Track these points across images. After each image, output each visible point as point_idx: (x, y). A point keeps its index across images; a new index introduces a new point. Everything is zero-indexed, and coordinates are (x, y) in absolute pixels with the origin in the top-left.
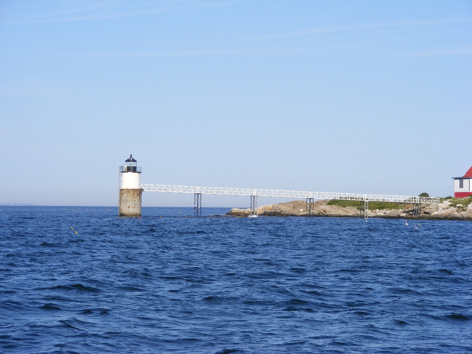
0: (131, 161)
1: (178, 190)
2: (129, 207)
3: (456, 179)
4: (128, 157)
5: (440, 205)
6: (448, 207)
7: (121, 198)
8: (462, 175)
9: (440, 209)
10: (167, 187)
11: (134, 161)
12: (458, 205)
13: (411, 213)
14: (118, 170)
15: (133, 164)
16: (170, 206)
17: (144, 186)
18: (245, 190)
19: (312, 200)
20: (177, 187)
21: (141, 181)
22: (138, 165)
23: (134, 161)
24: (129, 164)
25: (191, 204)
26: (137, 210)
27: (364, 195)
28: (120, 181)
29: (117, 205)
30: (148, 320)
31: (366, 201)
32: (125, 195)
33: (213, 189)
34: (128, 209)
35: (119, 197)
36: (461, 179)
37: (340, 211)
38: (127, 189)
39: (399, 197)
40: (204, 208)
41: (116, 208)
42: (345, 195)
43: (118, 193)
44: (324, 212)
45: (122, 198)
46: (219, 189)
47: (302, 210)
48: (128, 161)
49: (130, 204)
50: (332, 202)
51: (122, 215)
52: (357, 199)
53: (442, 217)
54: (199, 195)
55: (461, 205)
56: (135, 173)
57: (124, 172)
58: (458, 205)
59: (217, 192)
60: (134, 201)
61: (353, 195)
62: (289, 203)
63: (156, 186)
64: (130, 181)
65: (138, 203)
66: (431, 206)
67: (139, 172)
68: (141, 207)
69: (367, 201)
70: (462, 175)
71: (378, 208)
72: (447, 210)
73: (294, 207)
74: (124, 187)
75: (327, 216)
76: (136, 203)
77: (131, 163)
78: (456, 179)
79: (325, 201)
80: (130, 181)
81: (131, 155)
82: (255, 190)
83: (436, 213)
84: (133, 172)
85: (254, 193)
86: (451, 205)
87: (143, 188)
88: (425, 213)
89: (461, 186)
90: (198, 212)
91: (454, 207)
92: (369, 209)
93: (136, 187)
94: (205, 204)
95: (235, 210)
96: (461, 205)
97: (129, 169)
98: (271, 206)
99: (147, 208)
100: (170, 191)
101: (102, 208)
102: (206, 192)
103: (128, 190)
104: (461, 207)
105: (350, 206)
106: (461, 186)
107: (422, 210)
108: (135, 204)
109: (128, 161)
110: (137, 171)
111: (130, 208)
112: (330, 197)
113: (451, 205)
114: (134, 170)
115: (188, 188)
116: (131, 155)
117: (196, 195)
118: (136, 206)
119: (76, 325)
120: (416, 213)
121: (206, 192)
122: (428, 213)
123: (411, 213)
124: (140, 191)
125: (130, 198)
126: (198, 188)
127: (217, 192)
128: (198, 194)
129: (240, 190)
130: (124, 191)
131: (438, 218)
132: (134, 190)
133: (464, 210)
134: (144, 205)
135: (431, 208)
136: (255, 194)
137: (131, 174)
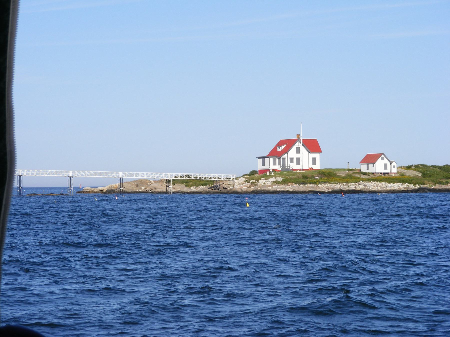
8: (265, 155)
9: (236, 185)
16: (28, 187)
20: (161, 174)
25: (115, 185)
27: (211, 175)
30: (421, 258)
36: (263, 158)
47: (143, 188)
50: (174, 181)
52: (201, 178)
54: (122, 179)
55: (254, 181)
59: (37, 174)
62: (133, 181)
73: (137, 185)
75: (228, 192)
78: (259, 158)
85: (70, 173)
86: (246, 181)
88: (224, 188)
89: (263, 164)
91: (248, 183)
95: (87, 189)
96: (254, 181)
101: (43, 188)
102: (27, 174)
106: (263, 164)
112: (170, 176)
113: (246, 181)
117: (119, 179)
119: (238, 253)
120: (216, 189)
122: (226, 188)
126: (169, 174)
129: (156, 174)
133: (256, 185)
136: (71, 176)
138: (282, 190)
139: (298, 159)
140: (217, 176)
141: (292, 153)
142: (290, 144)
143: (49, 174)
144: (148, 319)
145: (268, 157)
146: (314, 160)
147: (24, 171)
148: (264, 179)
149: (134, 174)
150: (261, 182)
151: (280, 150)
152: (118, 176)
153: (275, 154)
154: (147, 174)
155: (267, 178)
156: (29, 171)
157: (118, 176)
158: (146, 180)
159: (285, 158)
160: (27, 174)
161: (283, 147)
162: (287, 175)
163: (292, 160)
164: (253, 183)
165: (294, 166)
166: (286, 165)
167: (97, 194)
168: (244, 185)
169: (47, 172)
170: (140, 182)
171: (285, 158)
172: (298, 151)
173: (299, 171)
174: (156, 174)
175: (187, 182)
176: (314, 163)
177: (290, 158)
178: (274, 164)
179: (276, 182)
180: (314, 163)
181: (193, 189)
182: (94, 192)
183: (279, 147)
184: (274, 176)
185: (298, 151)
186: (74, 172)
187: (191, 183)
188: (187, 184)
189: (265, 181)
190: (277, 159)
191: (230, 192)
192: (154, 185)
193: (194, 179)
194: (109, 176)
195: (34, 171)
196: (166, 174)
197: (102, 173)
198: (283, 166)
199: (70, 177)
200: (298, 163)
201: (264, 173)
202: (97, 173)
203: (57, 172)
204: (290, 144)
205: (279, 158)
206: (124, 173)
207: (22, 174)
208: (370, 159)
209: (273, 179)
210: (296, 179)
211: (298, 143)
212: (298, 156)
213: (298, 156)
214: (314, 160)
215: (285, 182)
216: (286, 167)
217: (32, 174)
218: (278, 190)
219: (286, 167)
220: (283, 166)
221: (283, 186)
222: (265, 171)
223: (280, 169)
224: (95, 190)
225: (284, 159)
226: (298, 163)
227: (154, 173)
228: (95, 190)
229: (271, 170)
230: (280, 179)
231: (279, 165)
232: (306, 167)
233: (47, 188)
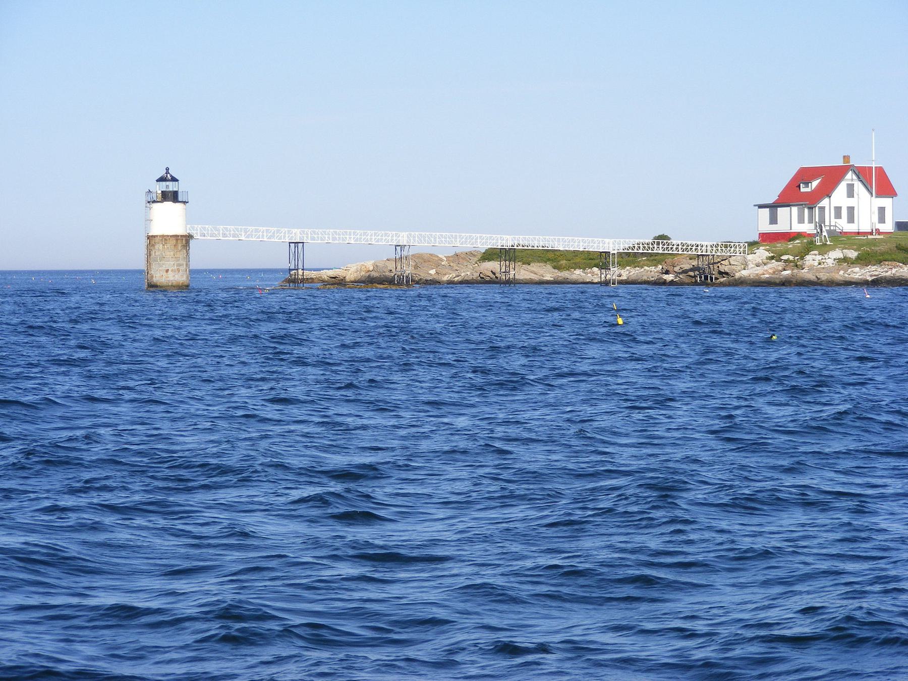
0: (168, 181)
2: (167, 271)
3: (761, 207)
4: (162, 173)
5: (750, 257)
6: (765, 261)
7: (149, 255)
8: (771, 200)
9: (751, 265)
11: (174, 179)
12: (785, 257)
13: (692, 274)
14: (143, 199)
15: (172, 187)
16: (234, 267)
21: (189, 220)
22: (180, 187)
23: (174, 179)
24: (163, 186)
25: (282, 262)
29: (142, 266)
30: (694, 592)
34: (165, 273)
35: (144, 251)
38: (163, 236)
41: (140, 272)
43: (144, 242)
45: (153, 253)
49: (170, 264)
50: (490, 255)
53: (778, 281)
54: (300, 245)
55: (791, 258)
56: (177, 204)
57: (154, 202)
58: (785, 257)
59: (334, 239)
60: (177, 259)
64: (168, 219)
67: (185, 202)
70: (772, 199)
72: (765, 268)
74: (155, 231)
76: (181, 262)
77: (168, 183)
78: (761, 207)
79: (472, 254)
80: (168, 219)
81: (167, 169)
82: (405, 234)
83: (745, 273)
86: (772, 258)
87: (193, 232)
89: (773, 220)
92: (619, 264)
93: (180, 231)
96: (791, 258)
100: (243, 238)
101: (38, 273)
103: (165, 238)
104: (791, 262)
105: (539, 262)
106: (773, 220)
110: (180, 199)
111: (169, 272)
112: (484, 244)
113: (772, 258)
114: (172, 197)
115: (278, 231)
116: (167, 169)
120: (705, 275)
121: (313, 239)
122: (727, 274)
123: (692, 274)
124: (188, 237)
125: (169, 254)
127: (334, 239)
130: (157, 240)
131: (741, 282)
132: (176, 236)
134: (194, 265)
135: (732, 263)
137: (169, 204)
142: (831, 177)
146: (882, 210)
151: (808, 190)
155: (824, 249)
158: (431, 255)
165: (844, 225)
172: (851, 193)
176: (882, 220)
177: (849, 208)
178: (801, 220)
180: (882, 220)
185: (851, 193)
189: (820, 257)
190: (806, 210)
200: (851, 220)
204: (831, 177)
205: (811, 209)
208: (808, 187)
209: (837, 254)
211: (850, 175)
212: (851, 202)
213: (851, 202)
214: (882, 210)
223: (815, 232)
225: (822, 209)
226: (851, 220)
231: (810, 221)
232: (865, 228)
233: (129, 271)
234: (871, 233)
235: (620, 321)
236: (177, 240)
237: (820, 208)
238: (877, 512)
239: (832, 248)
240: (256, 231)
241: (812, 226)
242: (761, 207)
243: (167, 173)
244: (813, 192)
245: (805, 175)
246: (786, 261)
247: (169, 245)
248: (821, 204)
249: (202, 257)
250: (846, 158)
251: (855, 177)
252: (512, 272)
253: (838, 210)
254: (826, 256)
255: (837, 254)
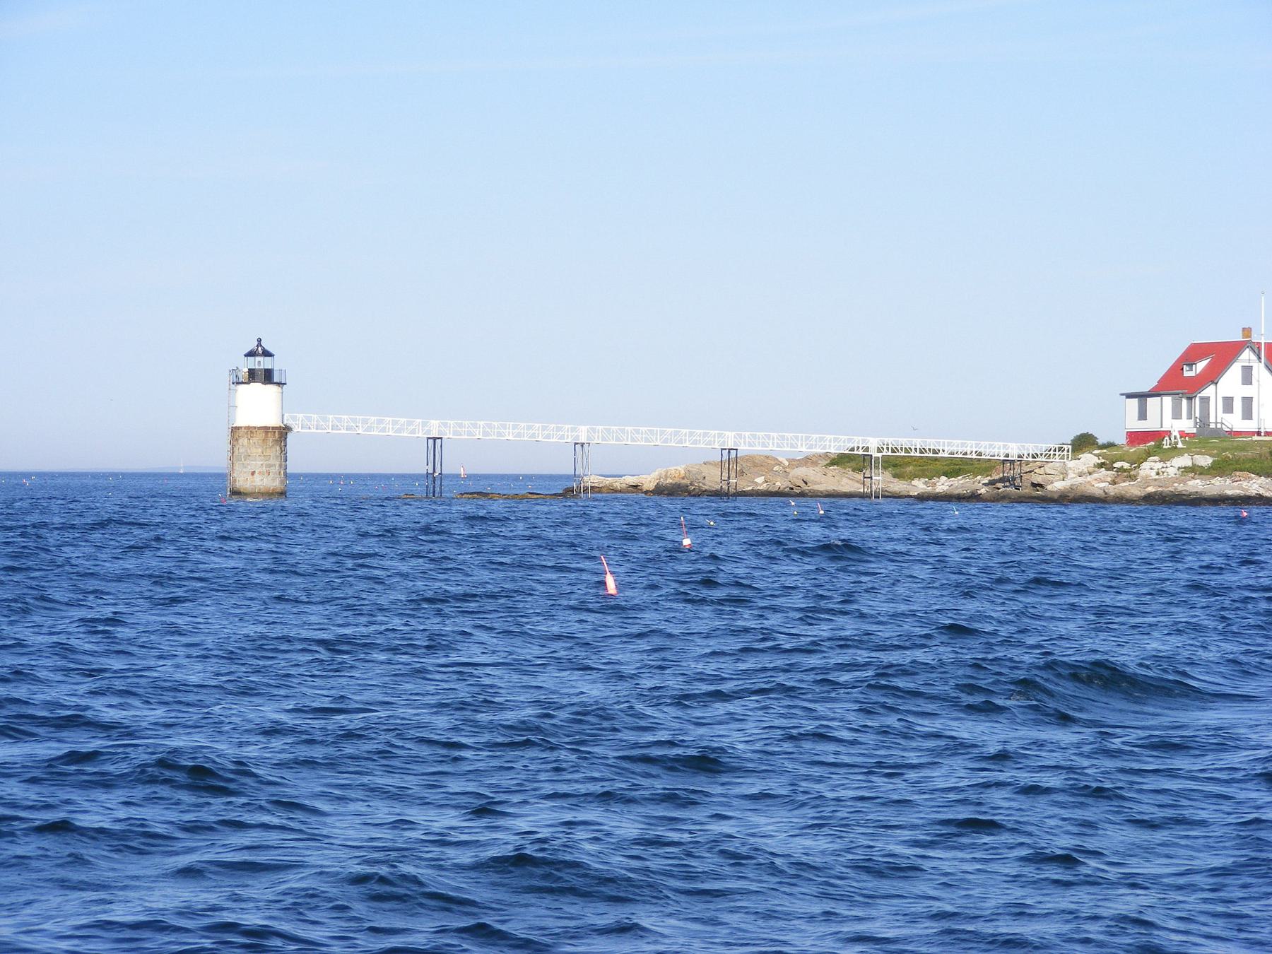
1: (383, 430)
2: (253, 473)
4: (252, 345)
5: (1071, 464)
6: (1091, 470)
8: (1146, 389)
9: (1071, 475)
10: (354, 420)
11: (266, 354)
14: (226, 378)
15: (265, 363)
17: (294, 418)
18: (559, 429)
19: (733, 453)
20: (821, 439)
23: (266, 354)
25: (419, 466)
26: (273, 480)
27: (871, 439)
28: (232, 407)
31: (875, 454)
32: (244, 441)
33: (475, 426)
34: (250, 477)
36: (1142, 396)
37: (845, 480)
38: (248, 428)
39: (991, 446)
40: (448, 476)
41: (221, 476)
42: (963, 445)
44: (802, 484)
46: (638, 432)
47: (760, 480)
48: (251, 354)
49: (257, 464)
50: (840, 460)
51: (235, 493)
53: (1056, 497)
54: (438, 441)
55: (1126, 465)
59: (486, 434)
60: (267, 458)
61: (931, 443)
63: (325, 420)
64: (258, 406)
65: (277, 463)
66: (1048, 468)
68: (285, 474)
69: (880, 455)
71: (945, 474)
74: (239, 423)
76: (272, 461)
77: (258, 359)
78: (1130, 396)
80: (258, 406)
81: (259, 340)
82: (584, 428)
84: (265, 383)
86: (1101, 466)
88: (1034, 485)
89: (1143, 415)
90: (434, 483)
91: (1107, 469)
93: (274, 421)
94: (455, 464)
97: (253, 376)
98: (681, 469)
99: (296, 476)
100: (687, 444)
103: (251, 430)
104: (1125, 471)
106: (1143, 415)
107: (1025, 477)
108: (270, 466)
109: (251, 354)
111: (257, 474)
112: (837, 446)
113: (1101, 466)
115: (705, 435)
116: (259, 340)
117: (431, 441)
118: (272, 470)
120: (1012, 488)
122: (1041, 486)
124: (282, 433)
125: (257, 451)
128: (435, 439)
130: (241, 432)
132: (266, 429)
138: (1242, 493)
139: (1248, 402)
140: (1014, 450)
141: (1230, 382)
143: (519, 435)
144: (116, 866)
145: (1158, 395)
147: (445, 425)
148: (1156, 458)
149: (768, 437)
150: (1149, 469)
151: (1192, 374)
152: (429, 431)
153: (1176, 384)
154: (807, 438)
156: (460, 426)
157: (429, 431)
158: (767, 457)
159: (1208, 398)
160: (455, 433)
161: (1201, 366)
162: (1225, 450)
163: (1228, 404)
164: (1121, 470)
165: (1235, 422)
166: (1212, 419)
167: (619, 495)
168: (1095, 476)
169: (515, 427)
170: (731, 461)
171: (1208, 398)
172: (1247, 377)
173: (1256, 438)
174: (691, 434)
175: (895, 466)
177: (1244, 398)
178: (1177, 415)
179: (1194, 470)
181: (919, 486)
182: (615, 491)
183: (1190, 365)
184: (1187, 450)
185: (1247, 377)
186: (594, 430)
187: (910, 468)
188: (897, 471)
189: (1159, 465)
190: (1184, 402)
191: (1071, 495)
192: (802, 472)
193: (918, 454)
194: (695, 442)
195: (475, 426)
196: (720, 435)
197: (676, 433)
198: (1203, 422)
199: (582, 445)
200: (1248, 414)
201: (1149, 442)
202: (662, 433)
203: (544, 429)
205: (1190, 399)
206: (740, 436)
207: (588, 438)
209: (1185, 461)
210: (1253, 460)
211: (1247, 355)
212: (1248, 391)
213: (1248, 391)
215: (1219, 469)
216: (1212, 426)
217: (470, 433)
218: (1229, 492)
219: (1212, 426)
220: (1203, 422)
221: (1218, 481)
222: (1158, 436)
223: (1194, 431)
224: (618, 483)
225: (1205, 401)
226: (1248, 414)
227: (684, 431)
228: (617, 485)
229: (1175, 433)
230: (1205, 461)
231: (1189, 417)
234: (1259, 434)
235: (687, 542)
236: (267, 433)
237: (1201, 398)
238: (89, 862)
239: (1180, 452)
240: (821, 439)
241: (1191, 422)
242: (1130, 396)
243: (259, 344)
244: (1198, 376)
245: (1193, 353)
246: (1119, 470)
247: (255, 440)
248: (1204, 393)
249: (302, 459)
250: (1247, 331)
251: (1253, 357)
252: (733, 481)
253: (1228, 404)
254: (1168, 464)
255: (1185, 461)
